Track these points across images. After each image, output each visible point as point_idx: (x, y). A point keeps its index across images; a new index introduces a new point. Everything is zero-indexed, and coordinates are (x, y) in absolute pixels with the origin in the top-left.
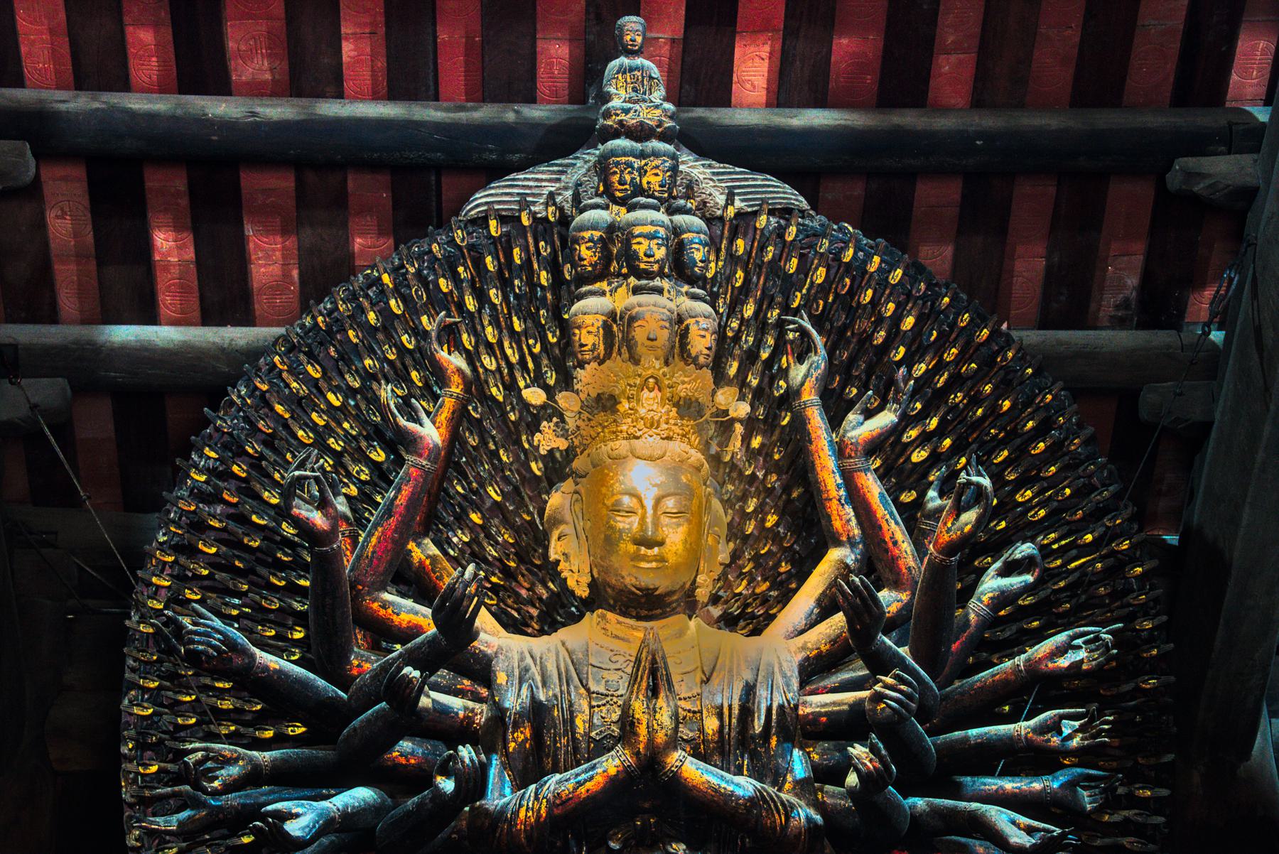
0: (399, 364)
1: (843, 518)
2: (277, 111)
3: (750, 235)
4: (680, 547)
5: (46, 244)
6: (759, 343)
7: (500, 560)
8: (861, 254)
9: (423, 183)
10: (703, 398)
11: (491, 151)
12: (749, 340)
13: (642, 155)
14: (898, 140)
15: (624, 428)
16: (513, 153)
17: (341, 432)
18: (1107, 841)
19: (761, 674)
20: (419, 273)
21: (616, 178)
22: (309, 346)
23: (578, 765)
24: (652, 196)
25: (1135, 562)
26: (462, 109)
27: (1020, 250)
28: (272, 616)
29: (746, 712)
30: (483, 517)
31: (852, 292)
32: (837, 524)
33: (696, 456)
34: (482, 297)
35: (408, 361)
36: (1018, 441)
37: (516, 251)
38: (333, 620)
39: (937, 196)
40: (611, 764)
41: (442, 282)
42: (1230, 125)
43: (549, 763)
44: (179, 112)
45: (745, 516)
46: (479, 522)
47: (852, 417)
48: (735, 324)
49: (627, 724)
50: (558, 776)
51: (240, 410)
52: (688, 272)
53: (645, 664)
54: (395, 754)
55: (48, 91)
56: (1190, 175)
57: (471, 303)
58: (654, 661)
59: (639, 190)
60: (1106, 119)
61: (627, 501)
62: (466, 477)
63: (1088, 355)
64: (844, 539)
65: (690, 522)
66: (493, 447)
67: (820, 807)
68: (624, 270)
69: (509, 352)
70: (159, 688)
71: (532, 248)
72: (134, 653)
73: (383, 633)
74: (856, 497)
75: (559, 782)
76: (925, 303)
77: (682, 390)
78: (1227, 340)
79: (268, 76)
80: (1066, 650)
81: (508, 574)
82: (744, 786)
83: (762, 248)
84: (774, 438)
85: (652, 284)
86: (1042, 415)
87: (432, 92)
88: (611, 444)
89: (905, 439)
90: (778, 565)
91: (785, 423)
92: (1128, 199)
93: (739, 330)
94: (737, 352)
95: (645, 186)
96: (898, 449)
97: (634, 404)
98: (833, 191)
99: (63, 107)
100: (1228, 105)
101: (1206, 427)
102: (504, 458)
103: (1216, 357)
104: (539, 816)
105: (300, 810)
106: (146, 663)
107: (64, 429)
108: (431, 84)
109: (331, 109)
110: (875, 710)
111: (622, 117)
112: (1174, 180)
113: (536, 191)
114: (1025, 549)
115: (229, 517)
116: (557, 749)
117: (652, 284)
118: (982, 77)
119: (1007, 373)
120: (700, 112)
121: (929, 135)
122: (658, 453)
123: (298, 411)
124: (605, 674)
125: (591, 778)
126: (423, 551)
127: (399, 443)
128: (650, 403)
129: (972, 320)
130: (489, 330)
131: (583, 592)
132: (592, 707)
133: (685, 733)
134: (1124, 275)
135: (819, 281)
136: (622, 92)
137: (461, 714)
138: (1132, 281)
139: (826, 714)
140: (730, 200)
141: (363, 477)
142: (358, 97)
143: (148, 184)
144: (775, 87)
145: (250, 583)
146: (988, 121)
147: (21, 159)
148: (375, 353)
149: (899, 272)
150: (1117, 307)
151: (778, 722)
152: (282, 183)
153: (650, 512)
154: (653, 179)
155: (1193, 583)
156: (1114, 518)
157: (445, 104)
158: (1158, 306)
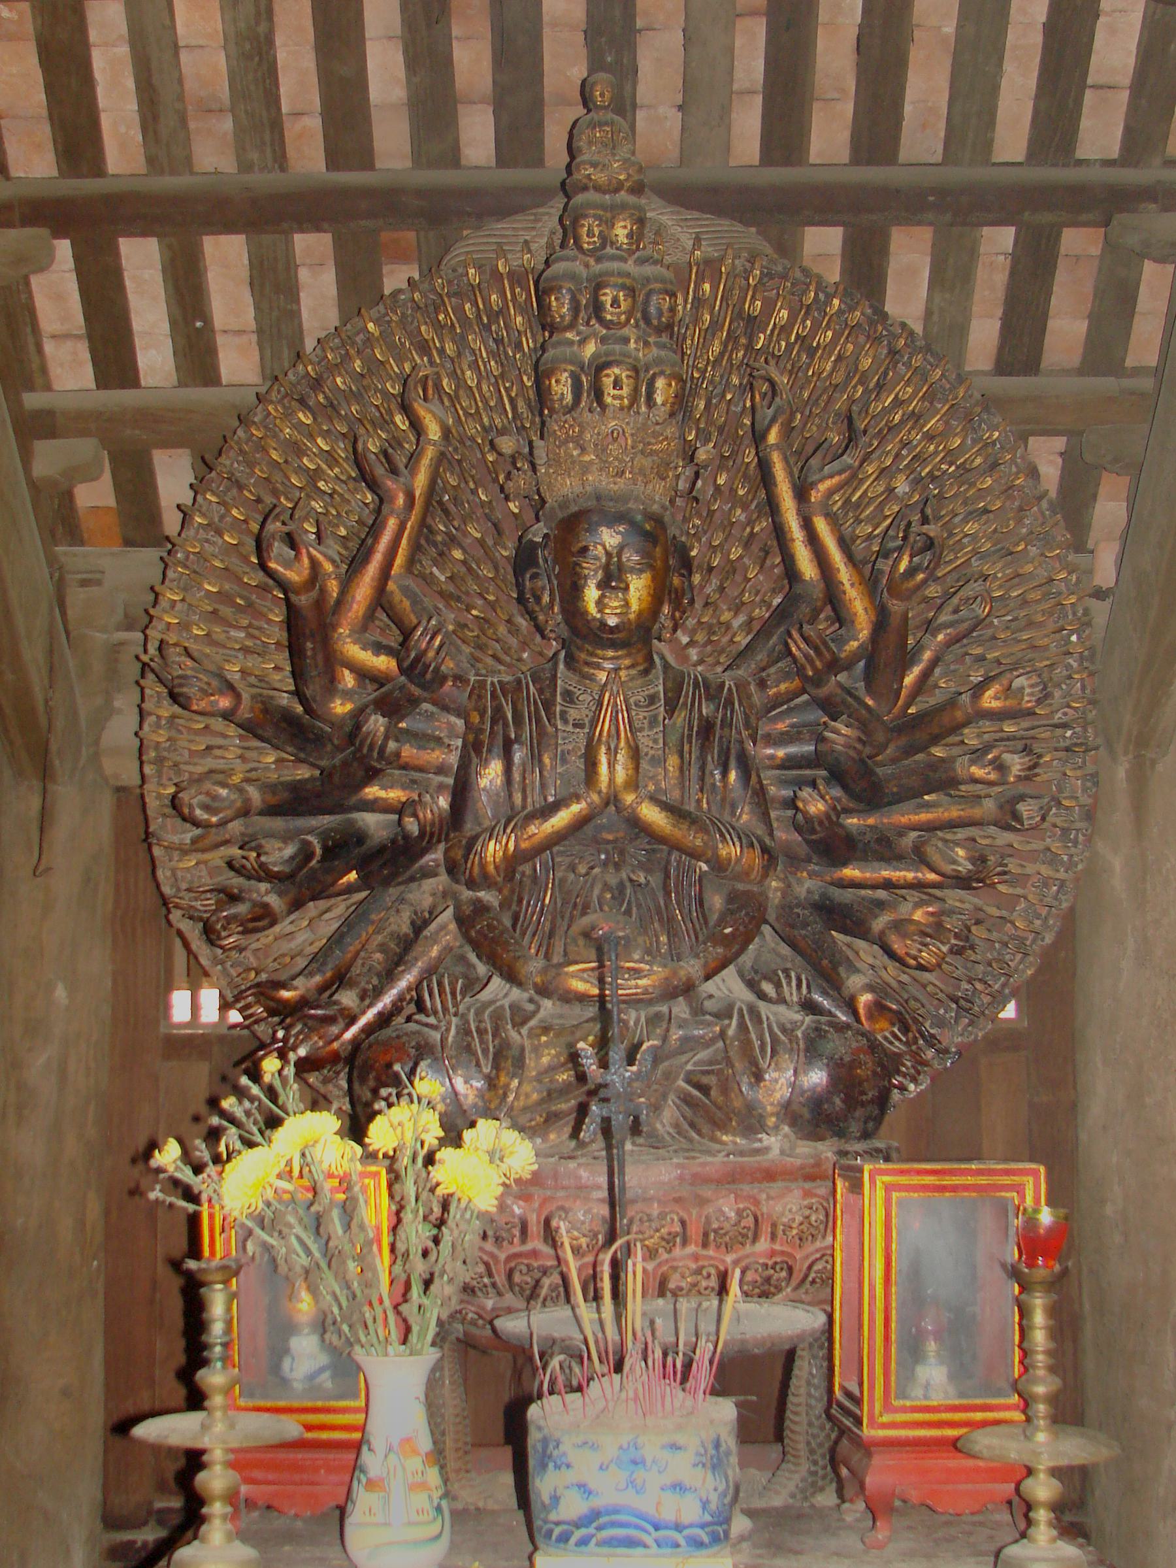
66: (472, 485)
113: (513, 240)
130: (468, 373)
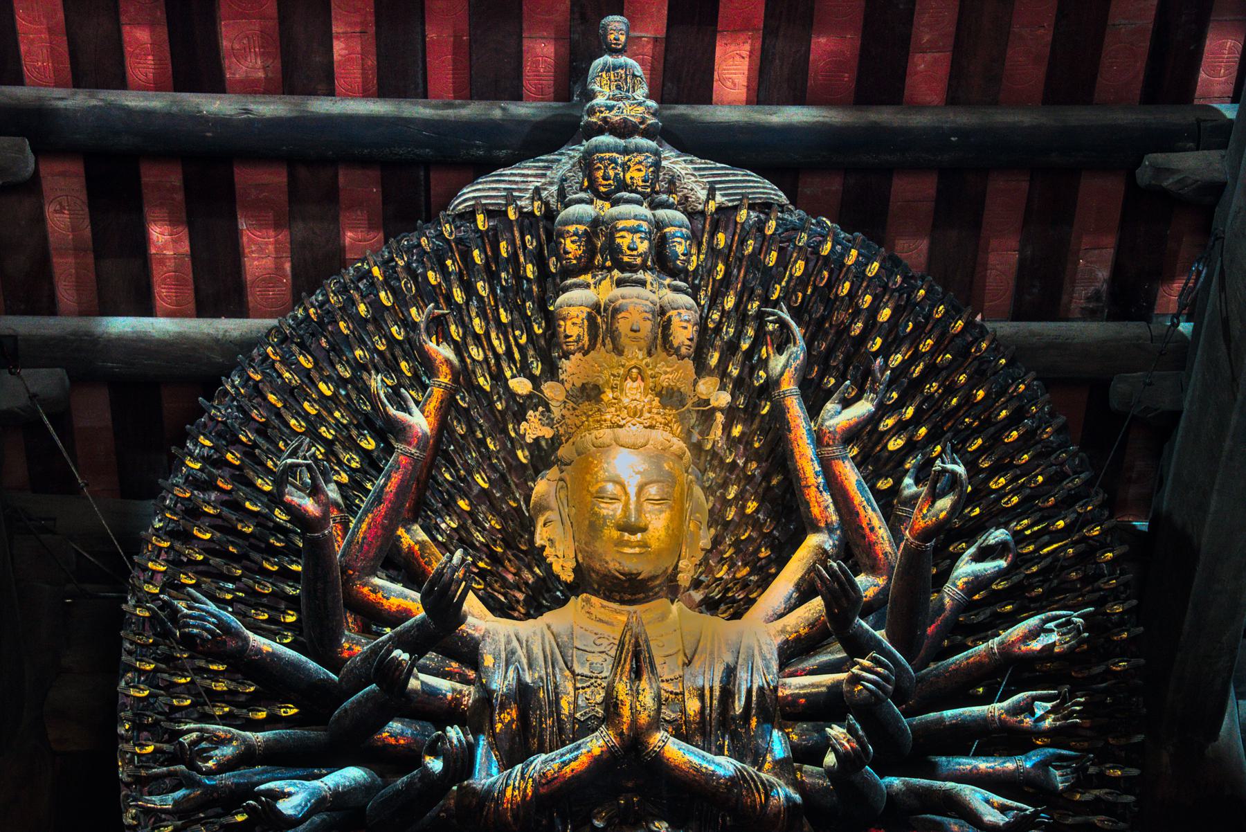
0: (388, 355)
1: (822, 504)
2: (270, 108)
3: (731, 229)
4: (663, 533)
5: (45, 238)
6: (739, 334)
7: (487, 546)
8: (838, 247)
9: (412, 178)
10: (685, 388)
11: (478, 147)
12: (729, 331)
13: (625, 151)
14: (875, 137)
15: (608, 417)
16: (500, 149)
17: (332, 421)
18: (1079, 819)
19: (742, 656)
20: (408, 266)
21: (600, 173)
22: (301, 337)
23: (564, 745)
24: (635, 191)
25: (1105, 547)
26: (450, 106)
27: (993, 243)
28: (265, 600)
29: (727, 694)
30: (471, 504)
31: (830, 285)
32: (816, 511)
33: (678, 444)
34: (469, 289)
35: (398, 352)
36: (992, 430)
37: (503, 245)
38: (324, 604)
39: (913, 191)
40: (595, 744)
41: (431, 274)
42: (1199, 121)
43: (535, 743)
44: (174, 109)
45: (726, 503)
46: (467, 508)
47: (830, 406)
48: (716, 316)
49: (611, 705)
50: (544, 756)
51: (233, 399)
52: (671, 265)
53: (629, 647)
54: (385, 735)
55: (47, 88)
56: (1160, 171)
57: (458, 296)
58: (637, 644)
59: (623, 185)
60: (1077, 116)
61: (610, 488)
62: (454, 465)
63: (1060, 346)
64: (823, 525)
65: (672, 508)
66: (480, 436)
67: (799, 786)
68: (608, 264)
69: (496, 343)
70: (155, 670)
71: (518, 242)
72: (131, 636)
73: (373, 617)
74: (834, 484)
75: (545, 762)
76: (901, 295)
77: (665, 380)
78: (1196, 331)
79: (261, 74)
80: (1039, 633)
81: (495, 559)
82: (724, 766)
83: (743, 242)
84: (754, 427)
85: (635, 276)
86: (1015, 404)
87: (420, 90)
88: (595, 432)
89: (881, 428)
90: (758, 550)
91: (764, 412)
92: (1099, 194)
93: (720, 322)
94: (718, 343)
95: (628, 181)
96: (875, 438)
97: (617, 394)
98: (811, 186)
99: (61, 104)
100: (1196, 102)
101: (1175, 416)
102: (491, 447)
103: (1184, 347)
104: (525, 795)
105: (292, 789)
106: (142, 646)
107: (62, 418)
108: (420, 81)
109: (322, 106)
110: (852, 692)
111: (606, 114)
112: (1144, 176)
113: (522, 186)
114: (998, 535)
115: (224, 503)
116: (542, 730)
117: (635, 276)
118: (957, 75)
119: (981, 364)
120: (682, 109)
121: (905, 132)
122: (641, 441)
123: (291, 400)
124: (590, 656)
125: (576, 758)
126: (412, 537)
127: (389, 432)
128: (634, 393)
129: (946, 312)
130: (477, 321)
131: (568, 576)
132: (576, 689)
133: (668, 714)
134: (1095, 267)
135: (798, 274)
136: (606, 90)
137: (449, 695)
138: (1103, 274)
139: (805, 696)
140: (711, 195)
141: (354, 465)
142: (349, 95)
143: (145, 180)
144: (755, 84)
145: (244, 568)
146: (962, 118)
147: (20, 155)
148: (366, 344)
149: (876, 265)
150: (1088, 299)
151: (758, 703)
152: (275, 178)
153: (633, 498)
154: (637, 175)
155: (1162, 568)
156: (1086, 505)
157: (434, 102)
158: (1128, 298)
